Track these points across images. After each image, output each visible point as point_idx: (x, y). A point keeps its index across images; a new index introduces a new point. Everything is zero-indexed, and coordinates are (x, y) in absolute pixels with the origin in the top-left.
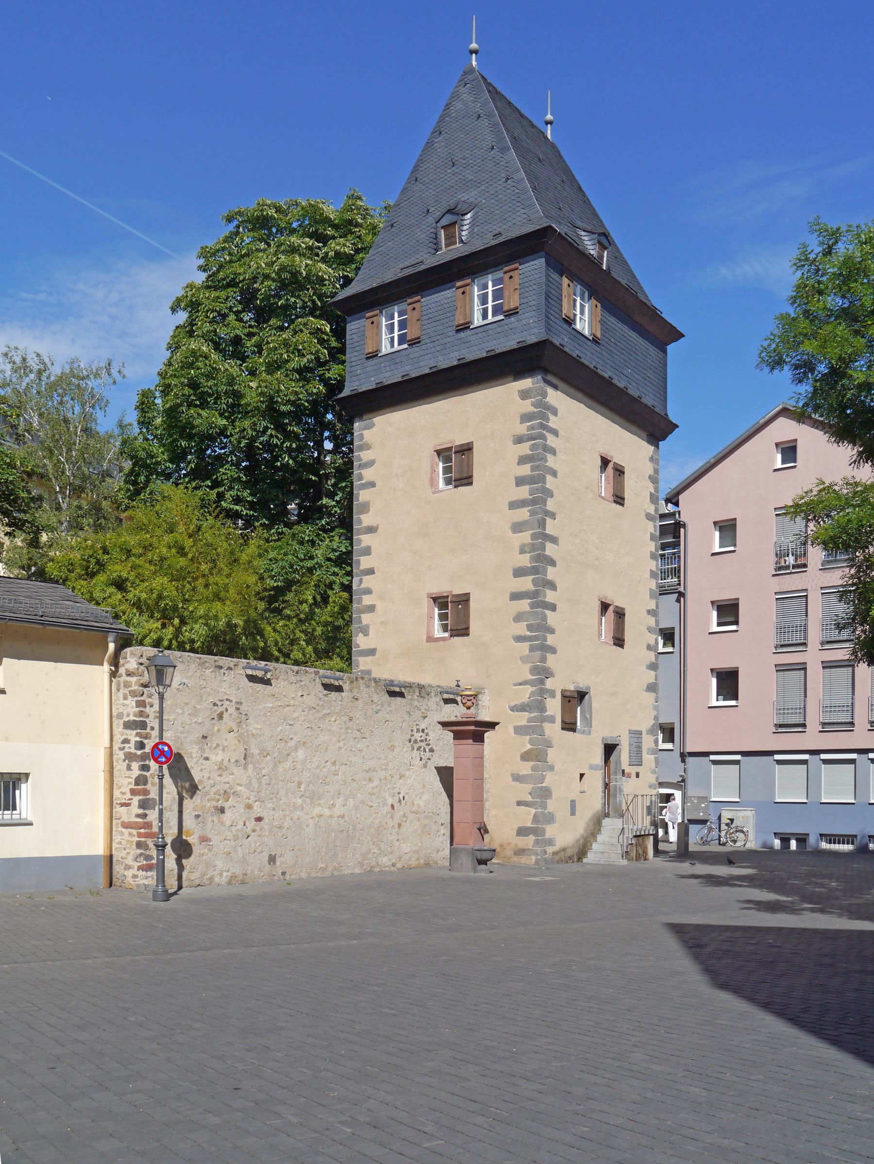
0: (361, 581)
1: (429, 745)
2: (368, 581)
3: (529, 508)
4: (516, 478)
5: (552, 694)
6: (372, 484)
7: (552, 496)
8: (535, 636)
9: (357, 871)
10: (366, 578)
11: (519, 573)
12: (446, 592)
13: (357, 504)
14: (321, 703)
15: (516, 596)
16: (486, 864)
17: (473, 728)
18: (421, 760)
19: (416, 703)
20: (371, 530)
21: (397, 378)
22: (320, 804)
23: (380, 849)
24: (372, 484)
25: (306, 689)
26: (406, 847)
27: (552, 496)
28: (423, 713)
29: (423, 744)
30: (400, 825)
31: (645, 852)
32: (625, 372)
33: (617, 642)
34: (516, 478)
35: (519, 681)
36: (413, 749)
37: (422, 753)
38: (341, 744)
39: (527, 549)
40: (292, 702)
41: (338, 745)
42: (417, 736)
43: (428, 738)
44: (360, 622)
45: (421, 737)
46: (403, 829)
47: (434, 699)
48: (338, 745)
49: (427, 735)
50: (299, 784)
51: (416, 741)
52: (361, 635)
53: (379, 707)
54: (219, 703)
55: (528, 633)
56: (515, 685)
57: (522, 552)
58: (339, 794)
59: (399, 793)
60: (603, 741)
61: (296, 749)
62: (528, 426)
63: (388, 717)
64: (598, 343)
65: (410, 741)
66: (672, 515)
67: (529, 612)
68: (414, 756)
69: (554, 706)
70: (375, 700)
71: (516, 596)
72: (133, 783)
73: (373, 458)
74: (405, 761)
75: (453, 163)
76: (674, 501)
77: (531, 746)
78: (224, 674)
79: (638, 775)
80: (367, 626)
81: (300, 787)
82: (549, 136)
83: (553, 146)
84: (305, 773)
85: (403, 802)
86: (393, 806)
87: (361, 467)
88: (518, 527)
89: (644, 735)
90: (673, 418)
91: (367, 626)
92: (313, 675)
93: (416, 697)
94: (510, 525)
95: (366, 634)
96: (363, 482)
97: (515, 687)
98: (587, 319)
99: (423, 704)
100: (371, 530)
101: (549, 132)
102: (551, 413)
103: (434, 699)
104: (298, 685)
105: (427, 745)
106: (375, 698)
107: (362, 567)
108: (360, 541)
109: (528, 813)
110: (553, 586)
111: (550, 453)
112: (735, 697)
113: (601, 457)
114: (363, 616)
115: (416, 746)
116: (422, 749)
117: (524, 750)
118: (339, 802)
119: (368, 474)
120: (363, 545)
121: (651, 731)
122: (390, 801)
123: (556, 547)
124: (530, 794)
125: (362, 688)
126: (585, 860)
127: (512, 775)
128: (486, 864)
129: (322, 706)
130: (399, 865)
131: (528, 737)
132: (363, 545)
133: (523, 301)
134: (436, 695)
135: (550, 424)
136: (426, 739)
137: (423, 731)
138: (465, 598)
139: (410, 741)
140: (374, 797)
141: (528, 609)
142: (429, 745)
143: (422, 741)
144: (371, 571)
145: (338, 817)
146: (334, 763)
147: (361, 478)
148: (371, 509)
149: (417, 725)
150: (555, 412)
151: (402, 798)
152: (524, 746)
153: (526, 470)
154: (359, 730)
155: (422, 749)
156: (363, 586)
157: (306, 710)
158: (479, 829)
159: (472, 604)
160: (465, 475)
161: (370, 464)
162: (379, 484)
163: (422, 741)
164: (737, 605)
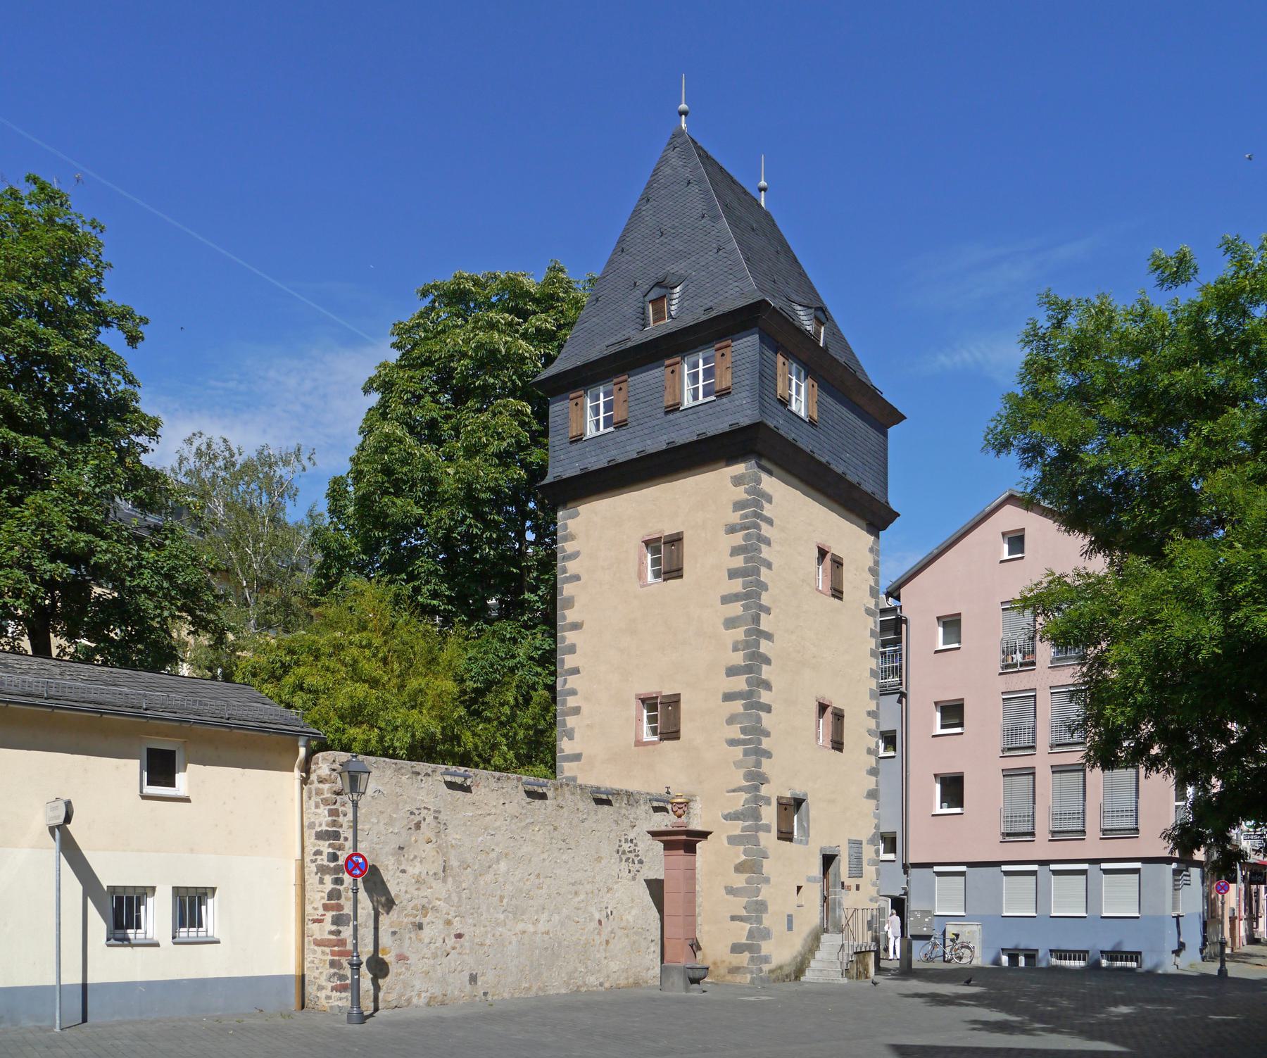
0: (565, 681)
1: (638, 856)
2: (572, 682)
4: (729, 570)
5: (768, 801)
6: (577, 578)
7: (767, 590)
8: (749, 739)
11: (732, 671)
12: (656, 693)
14: (524, 811)
15: (728, 697)
18: (629, 872)
19: (624, 811)
20: (576, 626)
21: (602, 463)
24: (577, 578)
26: (614, 966)
27: (767, 590)
31: (866, 970)
32: (843, 456)
34: (729, 570)
37: (630, 865)
38: (545, 855)
39: (740, 647)
40: (493, 811)
42: (626, 846)
43: (637, 849)
44: (565, 725)
49: (636, 845)
52: (565, 738)
53: (585, 816)
54: (417, 812)
55: (742, 736)
56: (728, 792)
57: (735, 649)
58: (544, 909)
59: (607, 908)
60: (821, 852)
62: (741, 515)
64: (816, 426)
65: (618, 852)
66: (893, 610)
68: (622, 867)
69: (770, 814)
71: (728, 697)
72: (326, 897)
73: (578, 549)
75: (662, 233)
76: (895, 595)
78: (422, 780)
79: (858, 888)
80: (572, 729)
82: (763, 204)
85: (611, 917)
86: (600, 922)
87: (565, 559)
88: (730, 623)
89: (864, 844)
90: (894, 504)
91: (572, 729)
94: (722, 620)
95: (571, 738)
96: (567, 575)
97: (728, 794)
100: (576, 626)
101: (763, 199)
103: (643, 807)
104: (499, 793)
106: (581, 806)
107: (566, 667)
108: (564, 638)
109: (743, 929)
110: (767, 686)
111: (765, 543)
112: (960, 804)
113: (819, 547)
114: (568, 718)
116: (631, 860)
117: (738, 861)
119: (572, 567)
120: (568, 642)
121: (872, 841)
122: (597, 916)
123: (771, 644)
124: (745, 908)
125: (567, 796)
126: (802, 979)
127: (726, 888)
129: (525, 814)
130: (607, 985)
131: (742, 848)
132: (568, 642)
133: (736, 380)
134: (645, 803)
135: (764, 513)
137: (631, 841)
138: (676, 699)
139: (618, 852)
141: (741, 710)
142: (638, 856)
143: (630, 852)
144: (576, 671)
146: (538, 876)
147: (565, 571)
148: (576, 604)
149: (625, 835)
150: (770, 500)
154: (564, 841)
155: (631, 860)
156: (567, 686)
157: (509, 819)
159: (683, 706)
160: (675, 568)
161: (575, 555)
163: (630, 852)
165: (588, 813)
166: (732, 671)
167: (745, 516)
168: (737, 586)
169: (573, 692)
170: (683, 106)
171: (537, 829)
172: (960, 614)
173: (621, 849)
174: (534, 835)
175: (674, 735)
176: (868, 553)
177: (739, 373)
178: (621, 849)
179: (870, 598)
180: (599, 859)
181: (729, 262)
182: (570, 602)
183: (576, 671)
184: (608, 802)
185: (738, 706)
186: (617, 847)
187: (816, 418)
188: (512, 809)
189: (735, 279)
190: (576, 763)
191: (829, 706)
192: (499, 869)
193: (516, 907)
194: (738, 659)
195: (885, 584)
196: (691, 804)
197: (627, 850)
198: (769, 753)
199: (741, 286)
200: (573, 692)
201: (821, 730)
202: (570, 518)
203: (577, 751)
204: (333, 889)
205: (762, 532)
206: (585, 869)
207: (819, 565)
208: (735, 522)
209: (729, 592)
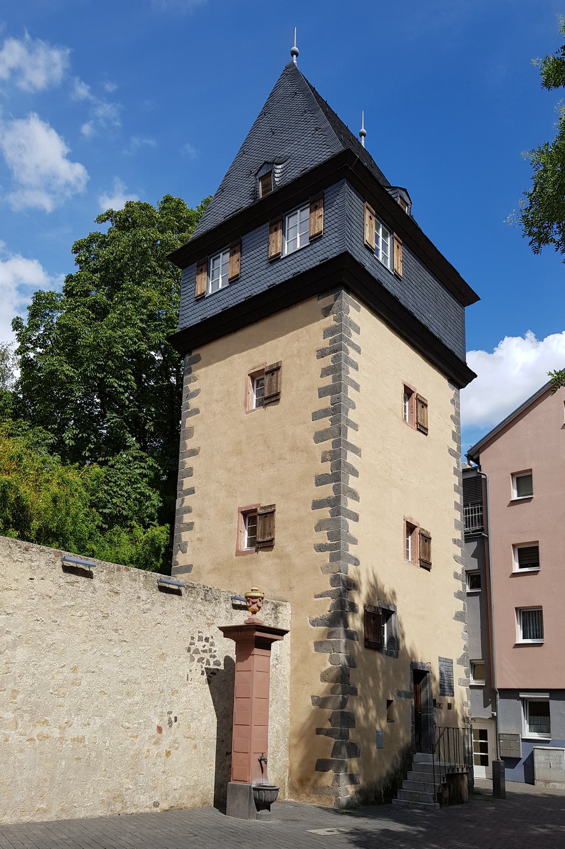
1: (214, 657)
3: (330, 417)
6: (197, 411)
9: (99, 813)
10: (187, 498)
11: (321, 480)
12: (253, 505)
13: (184, 431)
14: (60, 592)
15: (317, 505)
16: (269, 809)
17: (472, 735)
19: (199, 606)
20: (194, 453)
21: (218, 310)
22: (46, 721)
23: (136, 784)
24: (197, 411)
25: (38, 571)
26: (175, 782)
28: (208, 619)
29: (207, 656)
30: (168, 754)
33: (424, 564)
35: (319, 592)
36: (192, 659)
38: (87, 646)
40: (14, 585)
41: (83, 647)
42: (199, 645)
43: (213, 649)
45: (204, 646)
46: (173, 757)
47: (223, 605)
48: (83, 647)
49: (212, 644)
50: (15, 692)
51: (196, 651)
52: (180, 552)
53: (147, 606)
55: (329, 542)
56: (316, 597)
57: (324, 460)
58: (79, 710)
61: (14, 645)
63: (160, 618)
64: (400, 280)
65: (189, 650)
66: (474, 469)
67: (330, 520)
68: (193, 668)
70: (144, 597)
71: (317, 505)
73: (198, 388)
74: (181, 673)
76: (475, 457)
77: (331, 665)
80: (186, 543)
81: (15, 698)
82: (363, 145)
83: (365, 149)
84: (25, 679)
85: (174, 724)
86: (160, 729)
88: (320, 437)
91: (186, 543)
92: (53, 556)
93: (199, 600)
94: (313, 435)
95: (184, 552)
96: (189, 410)
97: (315, 599)
98: (389, 244)
99: (209, 609)
100: (194, 453)
101: (363, 141)
102: (353, 329)
103: (223, 605)
104: (26, 565)
105: (211, 656)
106: (143, 594)
108: (184, 463)
110: (355, 496)
111: (352, 366)
112: (540, 635)
113: (404, 385)
115: (197, 657)
116: (205, 661)
117: (324, 669)
118: (77, 721)
119: (193, 403)
120: (187, 466)
121: (461, 661)
122: (157, 722)
123: (358, 457)
124: (330, 720)
125: (124, 581)
126: (394, 801)
128: (269, 809)
129: (63, 595)
130: (164, 805)
131: (328, 655)
132: (187, 466)
133: (327, 225)
134: (226, 600)
135: (352, 339)
136: (210, 650)
137: (207, 640)
138: (270, 510)
139: (189, 650)
140: (132, 716)
141: (329, 516)
142: (214, 657)
143: (205, 651)
145: (73, 740)
146: (74, 669)
148: (195, 433)
149: (199, 632)
150: (358, 331)
151: (173, 719)
152: (325, 664)
153: (328, 381)
154: (116, 631)
155: (205, 661)
157: (37, 598)
158: (260, 761)
159: (277, 516)
162: (202, 410)
163: (205, 651)
164: (537, 548)
165: (153, 604)
166: (321, 480)
167: (334, 341)
168: (326, 402)
169: (189, 510)
170: (295, 48)
171: (78, 614)
172: (531, 470)
173: (193, 648)
174: (73, 621)
175: (268, 544)
176: (451, 404)
177: (329, 219)
178: (193, 648)
179: (453, 441)
180: (163, 657)
181: (324, 137)
182: (191, 432)
183: (192, 491)
184: (178, 593)
185: (326, 513)
186: (188, 645)
187: (401, 274)
188: (47, 586)
189: (328, 147)
190: (188, 574)
191: (416, 527)
192: (14, 657)
193: (37, 706)
194: (326, 468)
195: (467, 447)
196: (280, 608)
197: (201, 648)
198: (356, 559)
199: (332, 151)
200: (189, 510)
201: (410, 550)
202: (194, 363)
203: (189, 563)
204: (336, 742)
205: (349, 356)
206: (144, 666)
207: (405, 402)
208: (325, 347)
209: (319, 409)
